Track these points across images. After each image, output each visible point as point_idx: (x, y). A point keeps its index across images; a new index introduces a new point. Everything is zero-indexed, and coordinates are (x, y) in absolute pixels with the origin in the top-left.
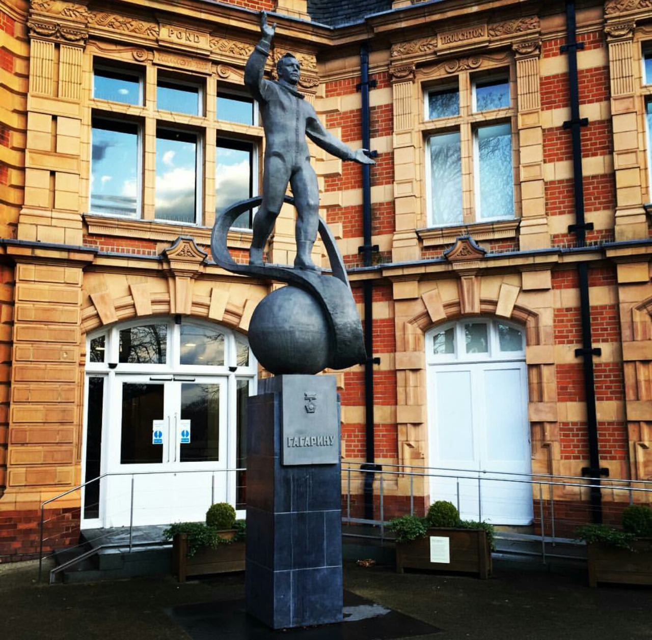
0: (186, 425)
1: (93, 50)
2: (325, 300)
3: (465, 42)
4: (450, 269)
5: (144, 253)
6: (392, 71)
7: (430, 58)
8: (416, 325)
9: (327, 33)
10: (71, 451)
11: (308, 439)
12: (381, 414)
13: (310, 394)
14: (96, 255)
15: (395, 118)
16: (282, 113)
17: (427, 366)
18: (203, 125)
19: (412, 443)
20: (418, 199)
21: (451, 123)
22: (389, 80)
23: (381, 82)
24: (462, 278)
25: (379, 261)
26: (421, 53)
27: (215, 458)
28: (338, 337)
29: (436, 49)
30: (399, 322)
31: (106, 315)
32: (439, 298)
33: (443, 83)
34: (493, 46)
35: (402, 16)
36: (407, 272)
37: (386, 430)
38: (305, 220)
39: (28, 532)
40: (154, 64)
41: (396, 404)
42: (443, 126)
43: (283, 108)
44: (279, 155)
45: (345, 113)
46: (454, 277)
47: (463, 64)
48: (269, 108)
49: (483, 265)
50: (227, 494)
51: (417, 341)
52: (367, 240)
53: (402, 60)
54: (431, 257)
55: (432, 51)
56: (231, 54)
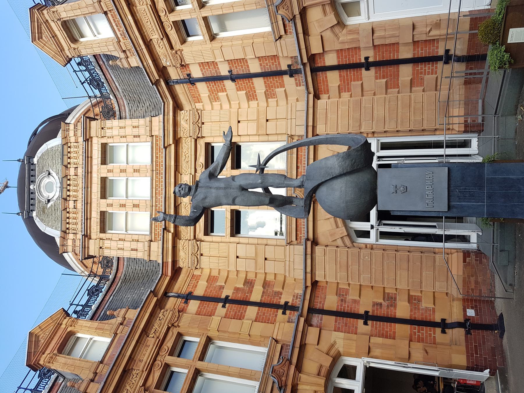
5: (304, 228)
6: (179, 65)
7: (165, 40)
12: (406, 53)
14: (307, 239)
15: (206, 61)
17: (371, 20)
19: (428, 29)
20: (254, 40)
23: (187, 71)
25: (297, 62)
29: (160, 39)
30: (338, 47)
31: (341, 233)
37: (418, 48)
39: (476, 282)
43: (205, 198)
45: (209, 91)
51: (351, 32)
54: (291, 26)
55: (161, 41)
56: (190, 162)
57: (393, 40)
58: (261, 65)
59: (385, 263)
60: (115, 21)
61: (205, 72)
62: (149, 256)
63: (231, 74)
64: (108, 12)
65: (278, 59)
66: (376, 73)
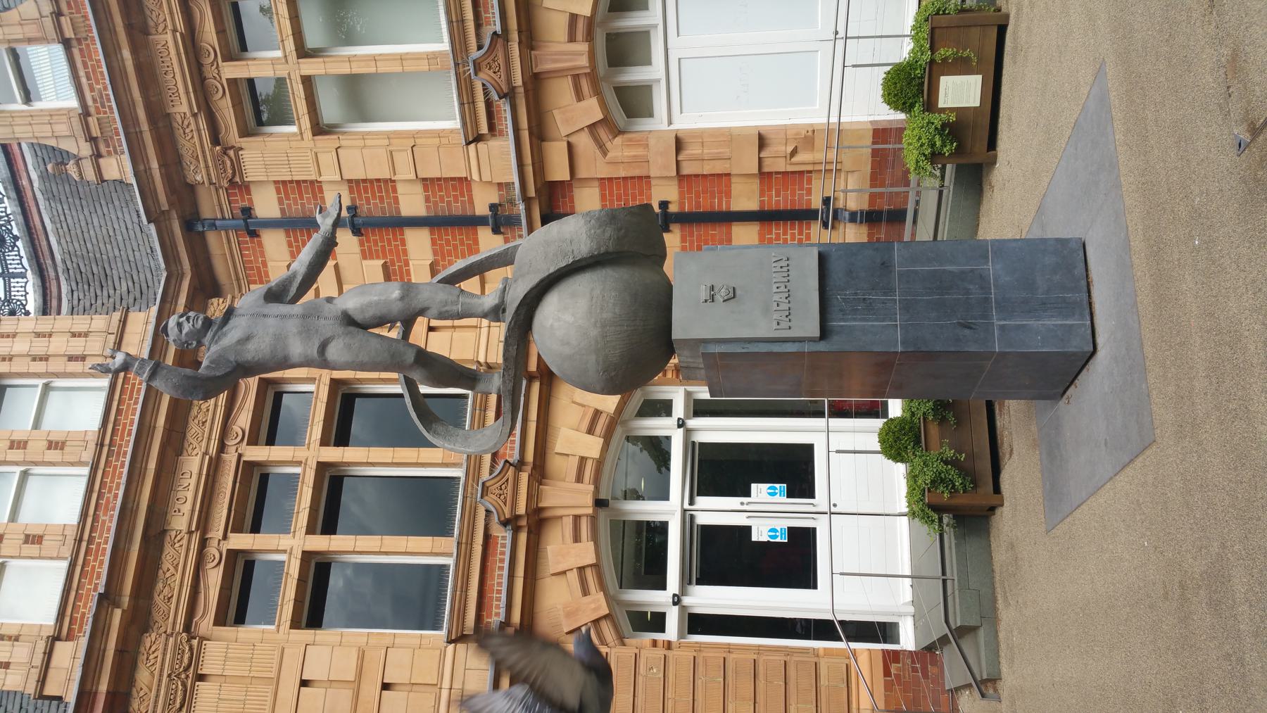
0: (760, 491)
1: (205, 624)
2: (552, 270)
3: (177, 70)
4: (522, 90)
7: (203, 124)
8: (608, 145)
9: (173, 281)
10: (797, 663)
11: (776, 298)
12: (745, 198)
13: (704, 294)
15: (296, 178)
16: (255, 340)
17: (672, 127)
18: (314, 466)
19: (790, 149)
21: (299, 90)
22: (238, 186)
23: (243, 200)
24: (535, 71)
25: (512, 202)
26: (196, 139)
27: (808, 450)
28: (611, 249)
29: (188, 114)
30: (604, 172)
32: (573, 113)
33: (241, 103)
34: (180, 25)
35: (142, 168)
36: (528, 160)
37: (770, 189)
38: (426, 305)
40: (225, 537)
41: (729, 175)
42: (304, 102)
43: (248, 338)
44: (323, 347)
46: (536, 82)
47: (210, 72)
48: (247, 362)
49: (515, 36)
50: (863, 433)
52: (482, 221)
53: (207, 167)
54: (504, 108)
55: (192, 120)
57: (718, 168)
58: (427, 200)
59: (698, 682)
60: (85, 66)
61: (289, 205)
62: (42, 681)
63: (354, 216)
64: (74, 43)
65: (469, 190)
66: (683, 240)
